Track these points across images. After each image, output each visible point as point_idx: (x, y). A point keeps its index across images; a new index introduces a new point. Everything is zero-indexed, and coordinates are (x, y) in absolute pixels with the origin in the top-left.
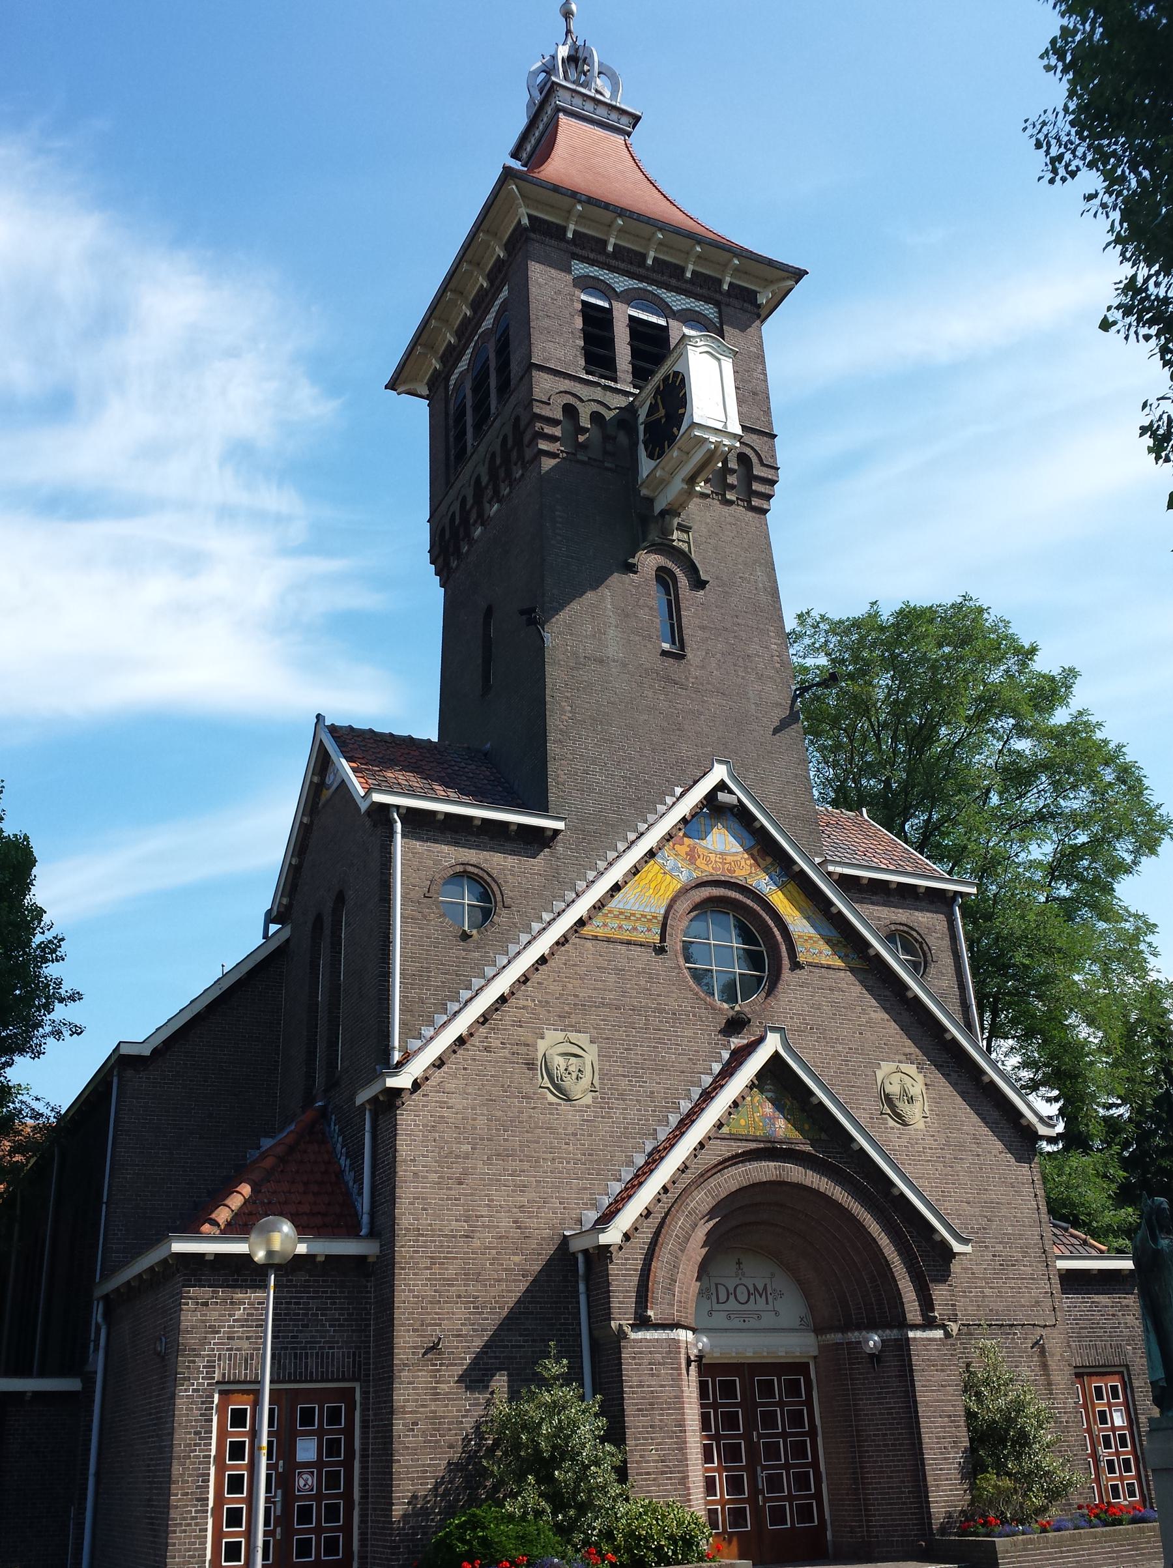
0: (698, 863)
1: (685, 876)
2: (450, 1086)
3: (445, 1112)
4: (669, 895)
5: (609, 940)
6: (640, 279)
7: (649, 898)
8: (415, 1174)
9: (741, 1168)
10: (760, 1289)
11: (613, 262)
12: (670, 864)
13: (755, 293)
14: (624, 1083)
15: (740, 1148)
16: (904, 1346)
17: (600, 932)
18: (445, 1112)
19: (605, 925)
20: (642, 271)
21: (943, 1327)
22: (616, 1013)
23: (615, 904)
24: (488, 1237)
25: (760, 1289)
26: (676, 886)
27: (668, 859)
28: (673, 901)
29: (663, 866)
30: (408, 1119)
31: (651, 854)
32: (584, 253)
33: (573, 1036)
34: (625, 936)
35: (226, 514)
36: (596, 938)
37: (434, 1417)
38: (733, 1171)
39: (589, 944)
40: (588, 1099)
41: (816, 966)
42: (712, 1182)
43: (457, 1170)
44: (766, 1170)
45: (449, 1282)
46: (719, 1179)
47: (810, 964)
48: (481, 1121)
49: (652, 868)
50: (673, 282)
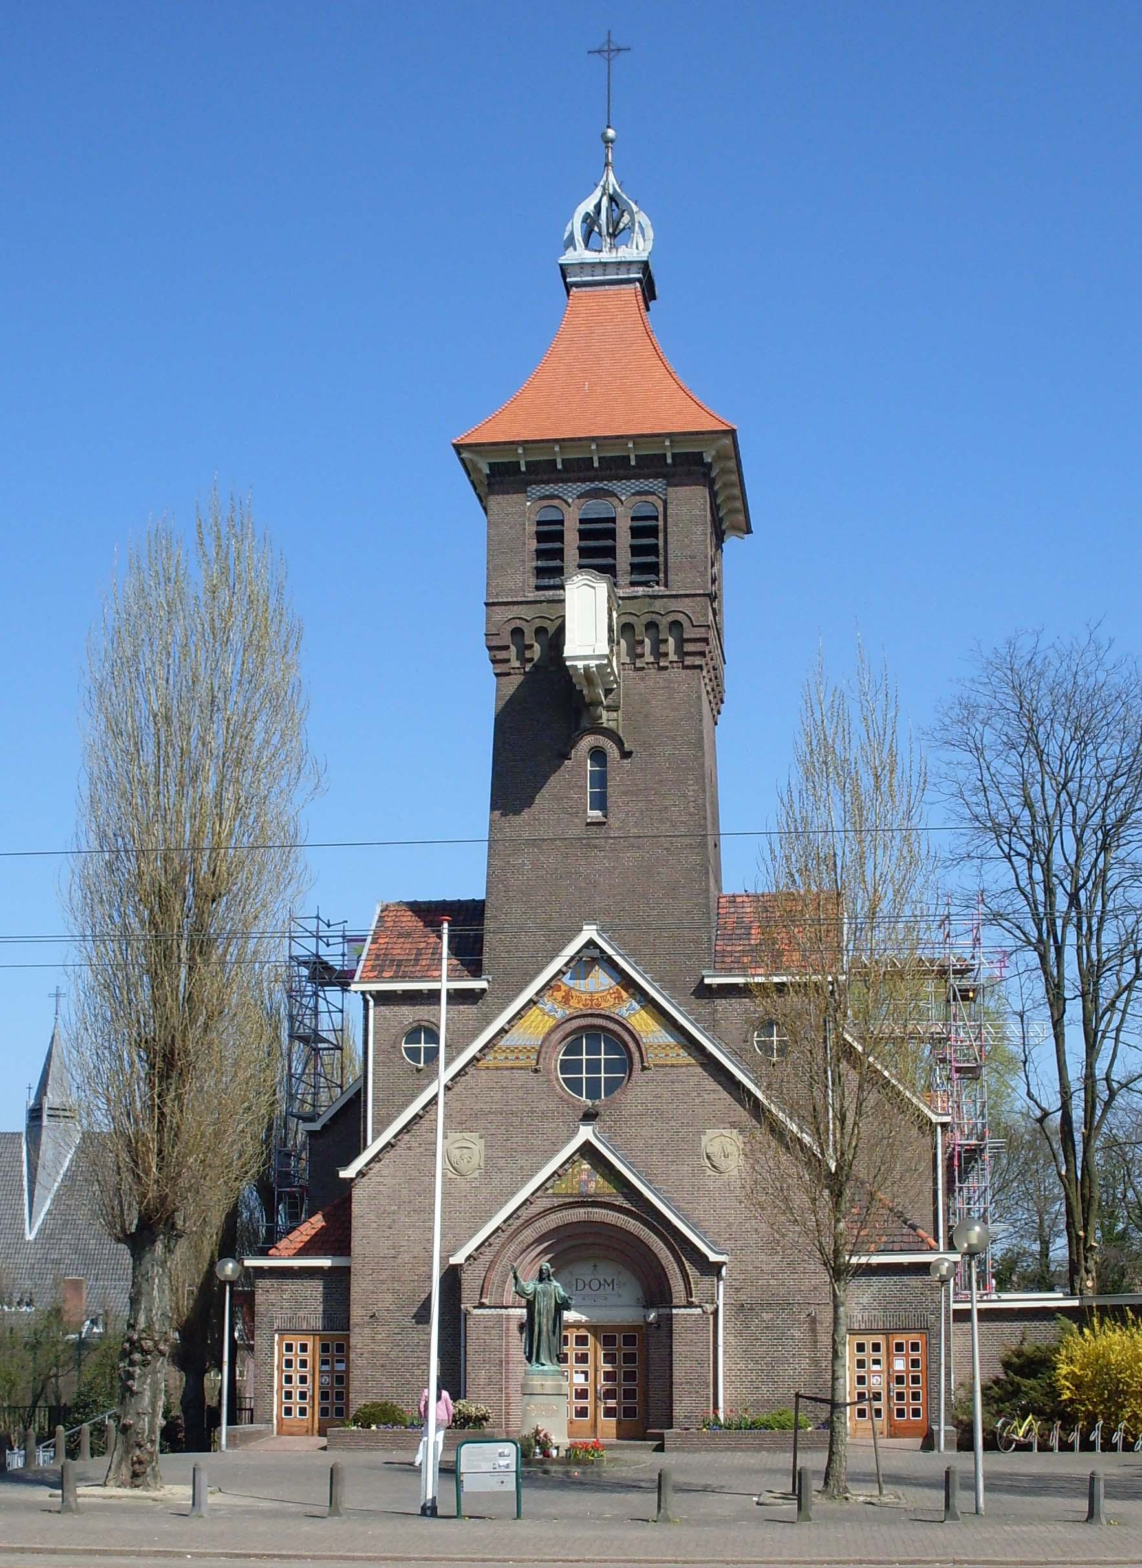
0: (571, 1003)
1: (561, 1013)
2: (385, 1172)
3: (381, 1188)
4: (546, 1030)
5: (497, 1068)
6: (592, 480)
7: (536, 1027)
8: (363, 1224)
9: (560, 1214)
10: (609, 1281)
11: (565, 476)
12: (547, 1008)
13: (701, 453)
14: (502, 1162)
15: (557, 1202)
16: (670, 1317)
17: (491, 1064)
18: (381, 1188)
19: (495, 1058)
20: (592, 473)
21: (701, 1307)
22: (500, 1117)
23: (504, 1042)
24: (406, 1257)
25: (609, 1281)
26: (551, 1023)
27: (547, 1003)
28: (549, 1034)
29: (542, 1010)
30: (357, 1193)
31: (532, 1003)
32: (539, 477)
33: (466, 1135)
34: (509, 1064)
35: (174, 1291)
36: (488, 1068)
37: (372, 1352)
38: (553, 1216)
39: (483, 1073)
40: (476, 1174)
41: (663, 1066)
42: (537, 1224)
43: (388, 1221)
44: (580, 1214)
45: (383, 1282)
46: (542, 1222)
47: (656, 1065)
48: (404, 1192)
49: (534, 1012)
50: (621, 472)
